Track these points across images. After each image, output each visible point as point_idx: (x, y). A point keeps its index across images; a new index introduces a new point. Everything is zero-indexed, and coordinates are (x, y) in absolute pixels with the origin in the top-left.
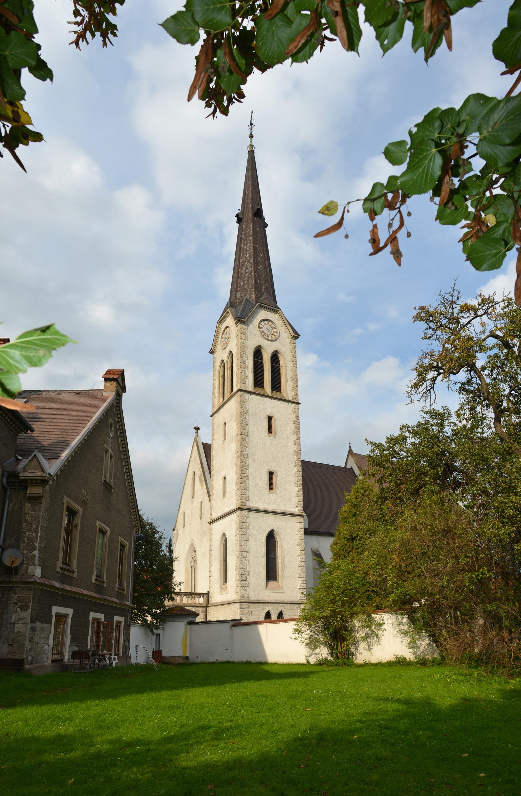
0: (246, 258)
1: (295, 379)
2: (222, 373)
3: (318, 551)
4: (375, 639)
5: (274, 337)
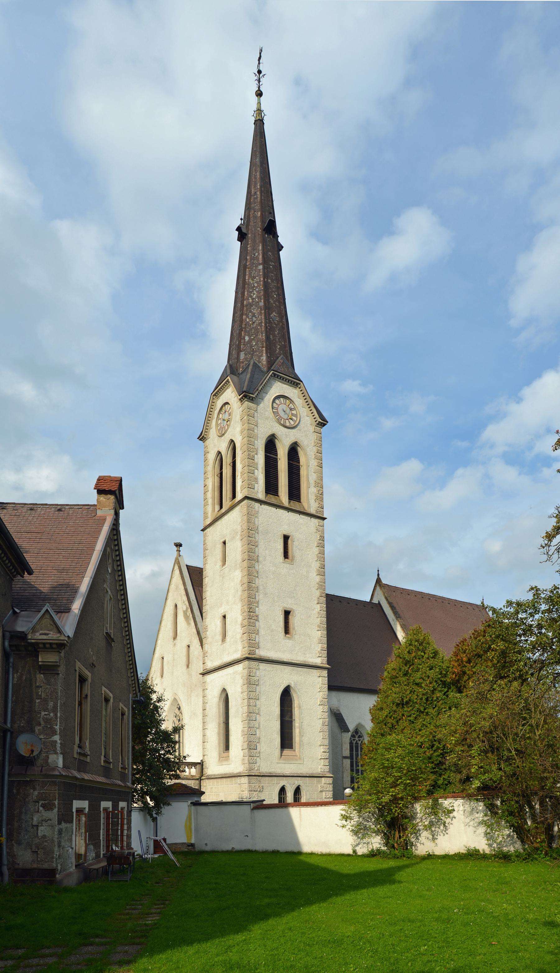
0: (253, 299)
1: (320, 485)
2: (217, 471)
3: (339, 710)
4: (442, 827)
5: (292, 422)
